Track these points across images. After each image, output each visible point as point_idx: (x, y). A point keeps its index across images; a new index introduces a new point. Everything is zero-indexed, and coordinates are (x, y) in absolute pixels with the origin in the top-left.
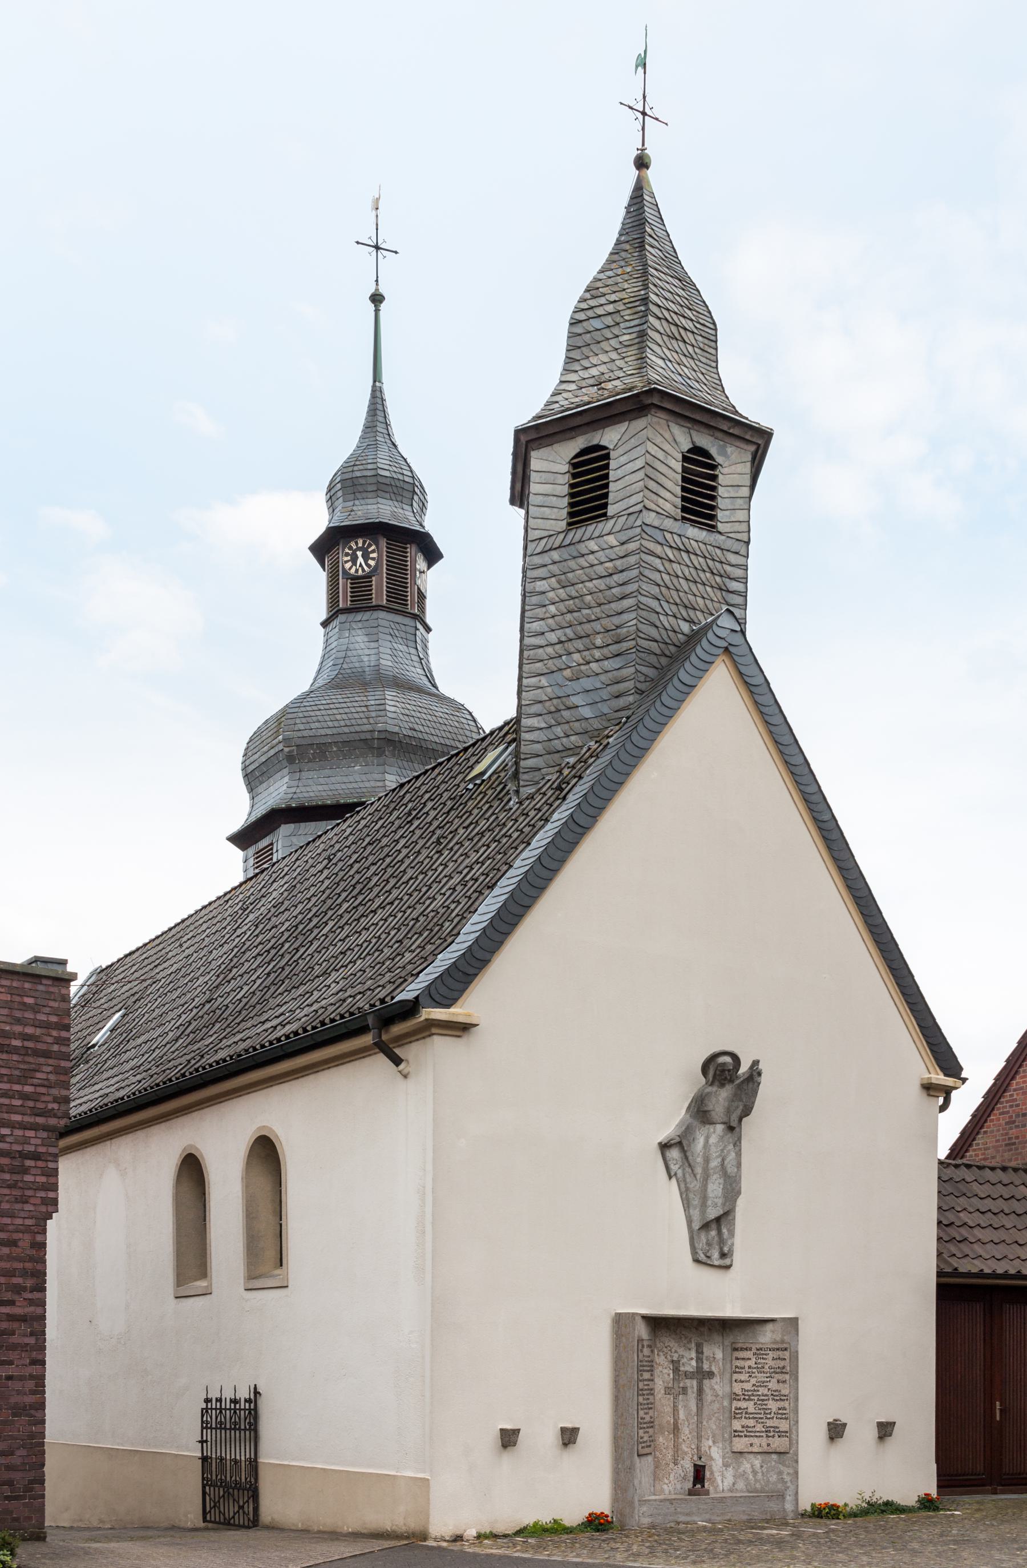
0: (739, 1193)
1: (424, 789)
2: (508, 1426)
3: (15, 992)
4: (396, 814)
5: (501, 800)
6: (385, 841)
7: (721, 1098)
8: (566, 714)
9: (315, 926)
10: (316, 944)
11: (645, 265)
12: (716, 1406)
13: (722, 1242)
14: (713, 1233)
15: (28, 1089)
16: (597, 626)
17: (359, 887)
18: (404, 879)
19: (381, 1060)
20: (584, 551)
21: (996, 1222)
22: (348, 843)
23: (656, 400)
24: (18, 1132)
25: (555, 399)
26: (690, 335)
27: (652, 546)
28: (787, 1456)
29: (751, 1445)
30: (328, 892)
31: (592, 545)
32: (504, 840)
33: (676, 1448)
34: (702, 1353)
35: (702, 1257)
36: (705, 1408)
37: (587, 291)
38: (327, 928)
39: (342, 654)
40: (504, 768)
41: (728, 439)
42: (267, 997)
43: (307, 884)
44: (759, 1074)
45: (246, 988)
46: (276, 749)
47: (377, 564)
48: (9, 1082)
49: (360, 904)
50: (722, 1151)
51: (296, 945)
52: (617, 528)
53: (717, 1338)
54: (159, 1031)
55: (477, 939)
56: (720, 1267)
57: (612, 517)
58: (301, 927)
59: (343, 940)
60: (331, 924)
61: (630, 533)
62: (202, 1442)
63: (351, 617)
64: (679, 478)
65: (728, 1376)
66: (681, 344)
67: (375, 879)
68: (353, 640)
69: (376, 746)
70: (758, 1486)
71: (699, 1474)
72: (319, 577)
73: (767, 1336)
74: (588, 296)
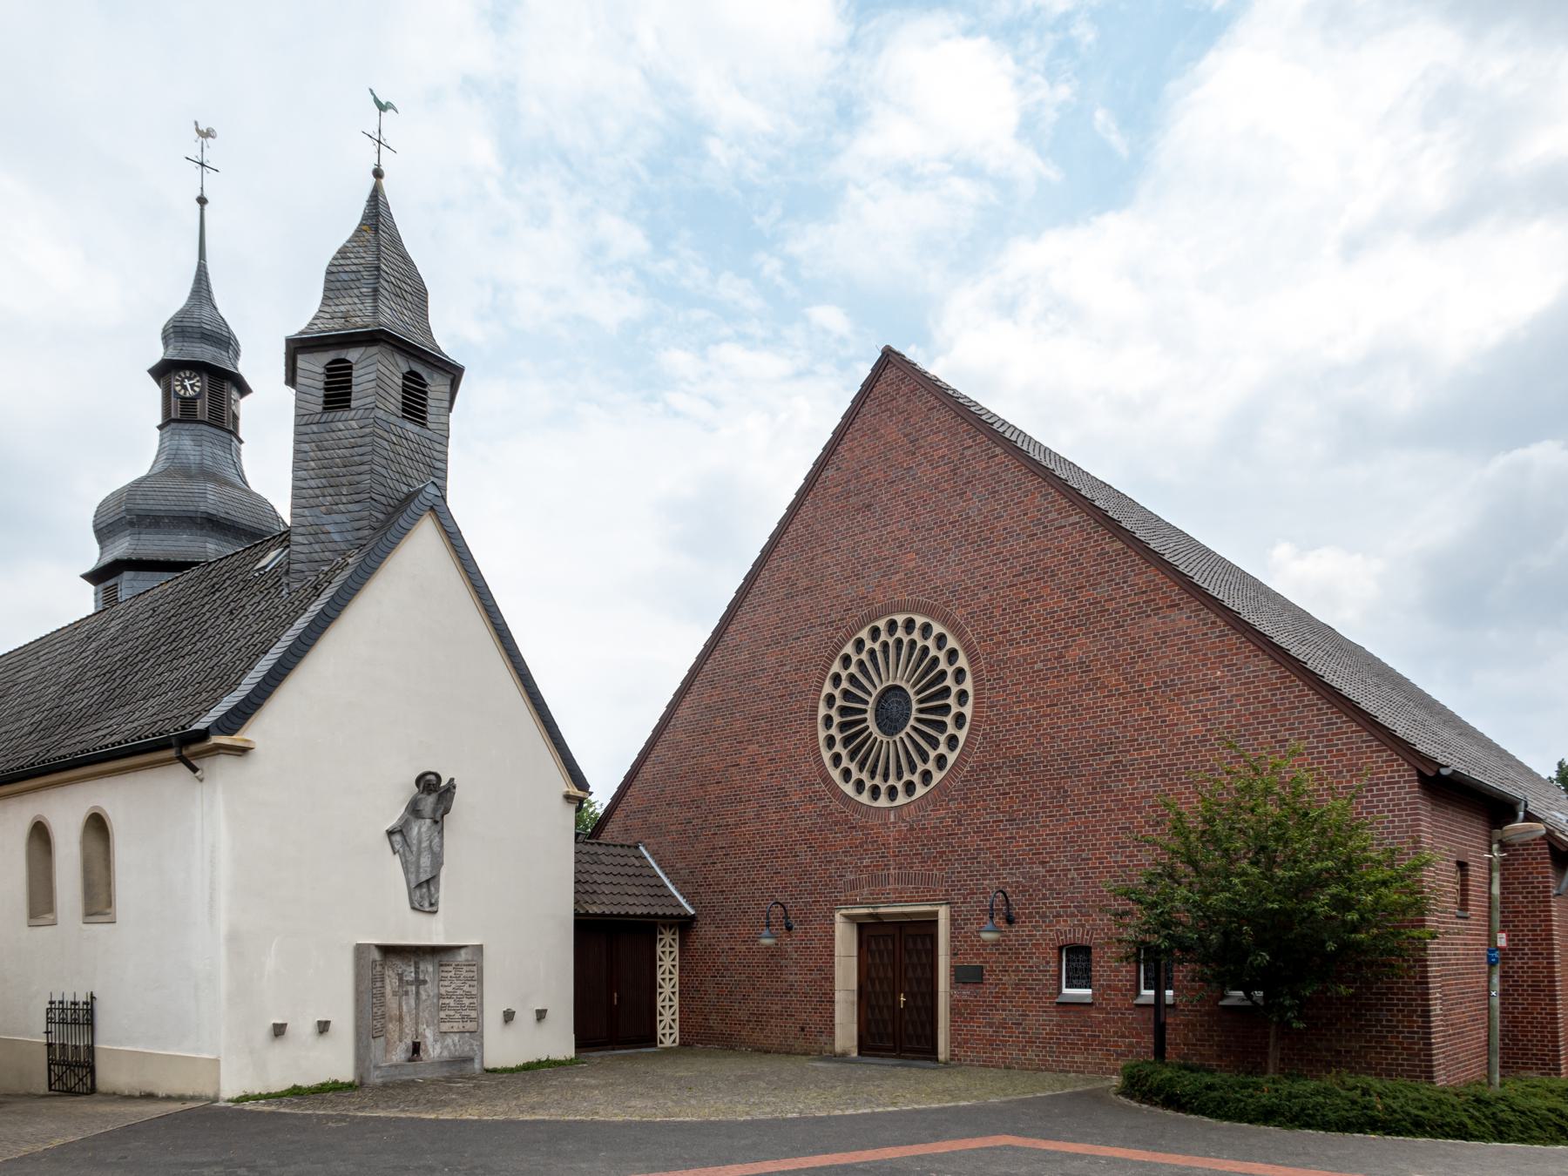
0: (442, 864)
1: (225, 569)
2: (279, 1021)
4: (204, 584)
5: (277, 589)
6: (195, 603)
7: (429, 802)
9: (140, 661)
10: (140, 674)
12: (429, 1002)
13: (430, 896)
14: (424, 890)
16: (344, 480)
17: (174, 636)
18: (205, 636)
19: (182, 768)
21: (615, 880)
22: (168, 600)
23: (383, 337)
25: (317, 322)
27: (381, 432)
28: (477, 1034)
30: (151, 635)
31: (341, 425)
32: (277, 619)
33: (401, 1031)
35: (417, 906)
37: (338, 253)
38: (149, 664)
39: (174, 452)
40: (280, 565)
42: (100, 710)
43: (137, 626)
44: (454, 787)
45: (86, 701)
46: (121, 516)
49: (173, 649)
51: (125, 673)
54: (17, 725)
55: (253, 690)
56: (430, 912)
58: (130, 659)
59: (160, 675)
60: (152, 661)
61: (367, 421)
62: (47, 1032)
63: (181, 425)
64: (401, 390)
65: (436, 983)
67: (186, 632)
68: (182, 442)
71: (416, 1048)
72: (155, 392)
73: (463, 956)
74: (339, 256)
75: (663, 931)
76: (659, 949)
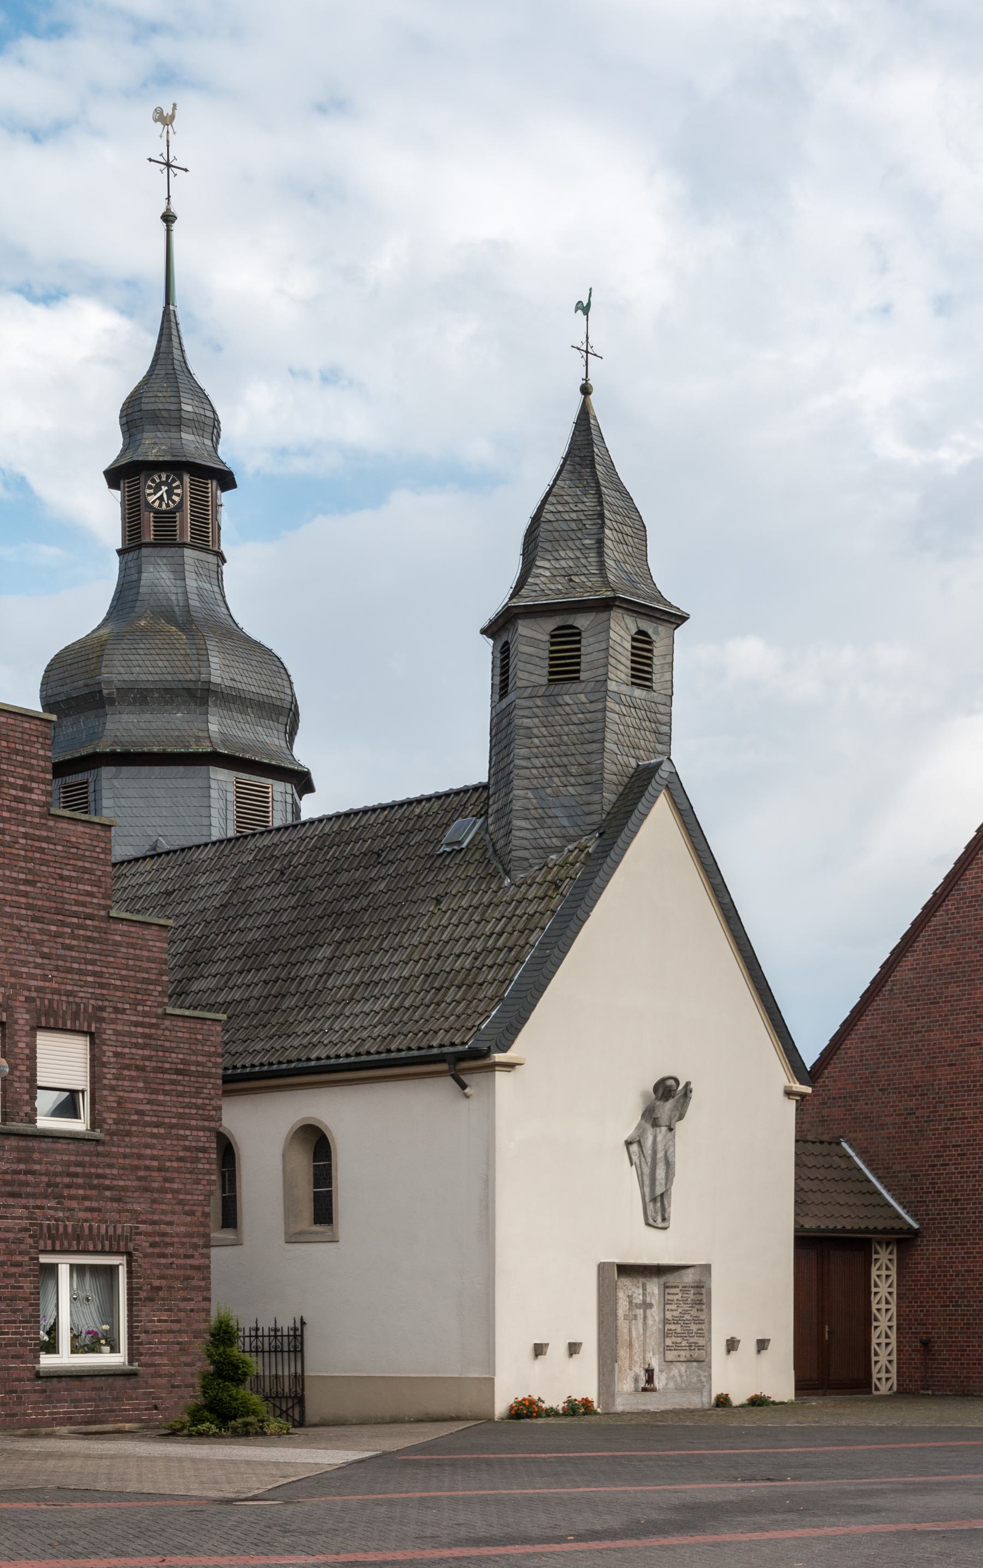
3: (191, 1031)
8: (549, 821)
11: (597, 483)
15: (200, 1101)
19: (450, 1081)
20: (561, 702)
24: (195, 1133)
26: (630, 538)
29: (679, 1356)
31: (567, 699)
33: (631, 1357)
34: (646, 1290)
35: (651, 1221)
36: (648, 1330)
41: (659, 622)
47: (182, 500)
48: (190, 1097)
50: (665, 1145)
52: (588, 689)
53: (655, 1280)
57: (583, 681)
65: (662, 1306)
66: (625, 546)
69: (199, 696)
70: (683, 1385)
73: (689, 1278)
75: (879, 1248)
76: (874, 1272)
